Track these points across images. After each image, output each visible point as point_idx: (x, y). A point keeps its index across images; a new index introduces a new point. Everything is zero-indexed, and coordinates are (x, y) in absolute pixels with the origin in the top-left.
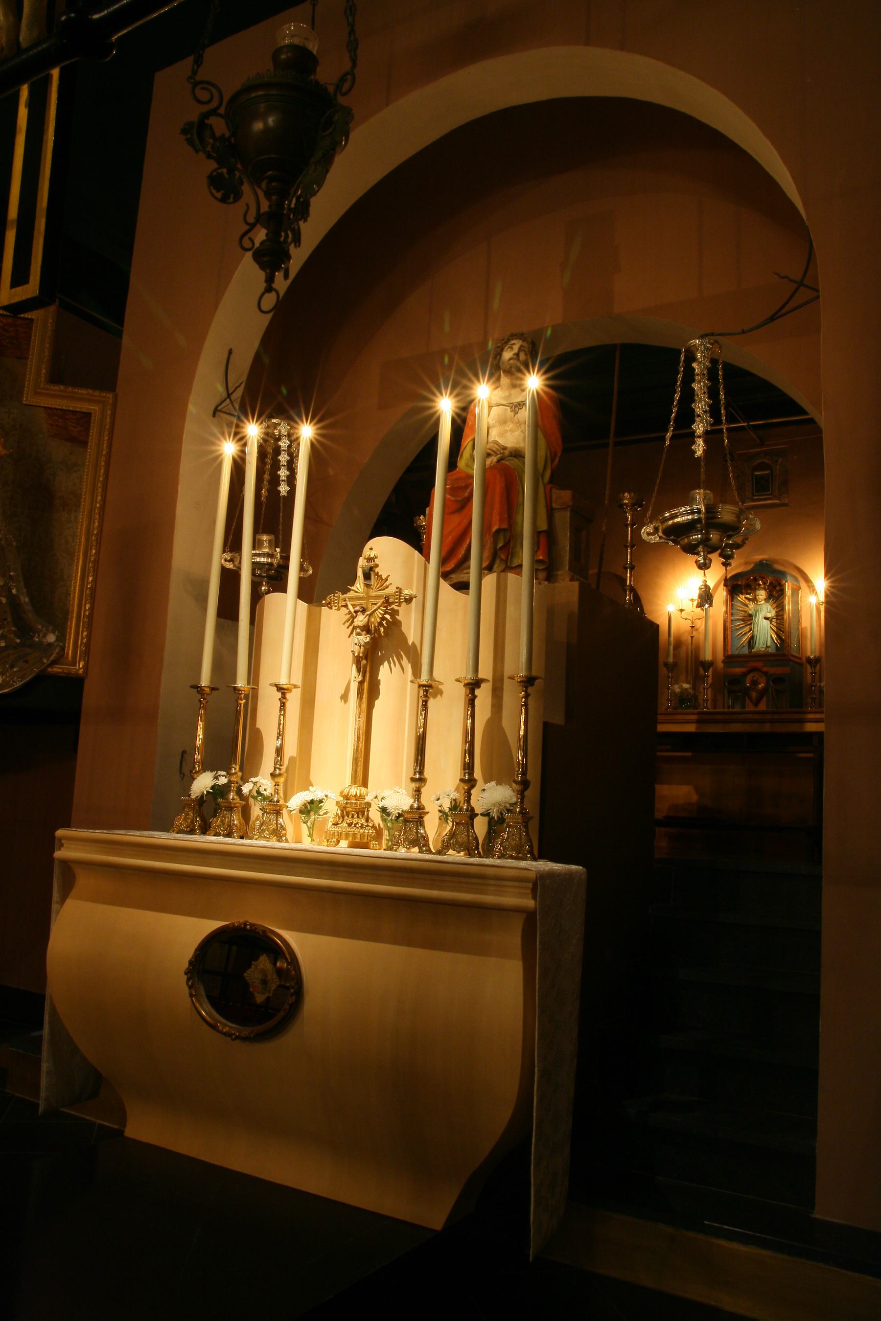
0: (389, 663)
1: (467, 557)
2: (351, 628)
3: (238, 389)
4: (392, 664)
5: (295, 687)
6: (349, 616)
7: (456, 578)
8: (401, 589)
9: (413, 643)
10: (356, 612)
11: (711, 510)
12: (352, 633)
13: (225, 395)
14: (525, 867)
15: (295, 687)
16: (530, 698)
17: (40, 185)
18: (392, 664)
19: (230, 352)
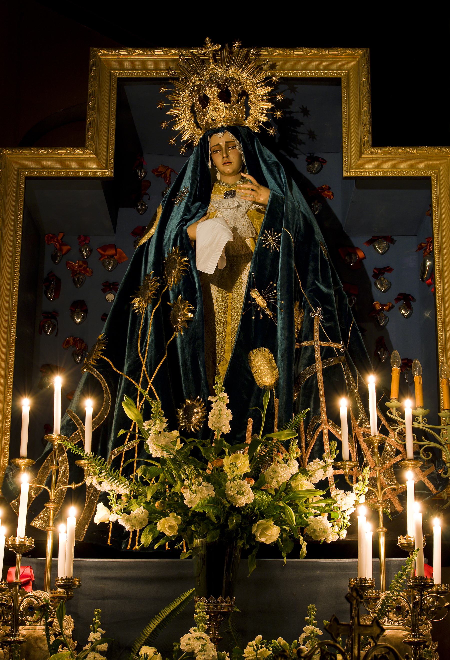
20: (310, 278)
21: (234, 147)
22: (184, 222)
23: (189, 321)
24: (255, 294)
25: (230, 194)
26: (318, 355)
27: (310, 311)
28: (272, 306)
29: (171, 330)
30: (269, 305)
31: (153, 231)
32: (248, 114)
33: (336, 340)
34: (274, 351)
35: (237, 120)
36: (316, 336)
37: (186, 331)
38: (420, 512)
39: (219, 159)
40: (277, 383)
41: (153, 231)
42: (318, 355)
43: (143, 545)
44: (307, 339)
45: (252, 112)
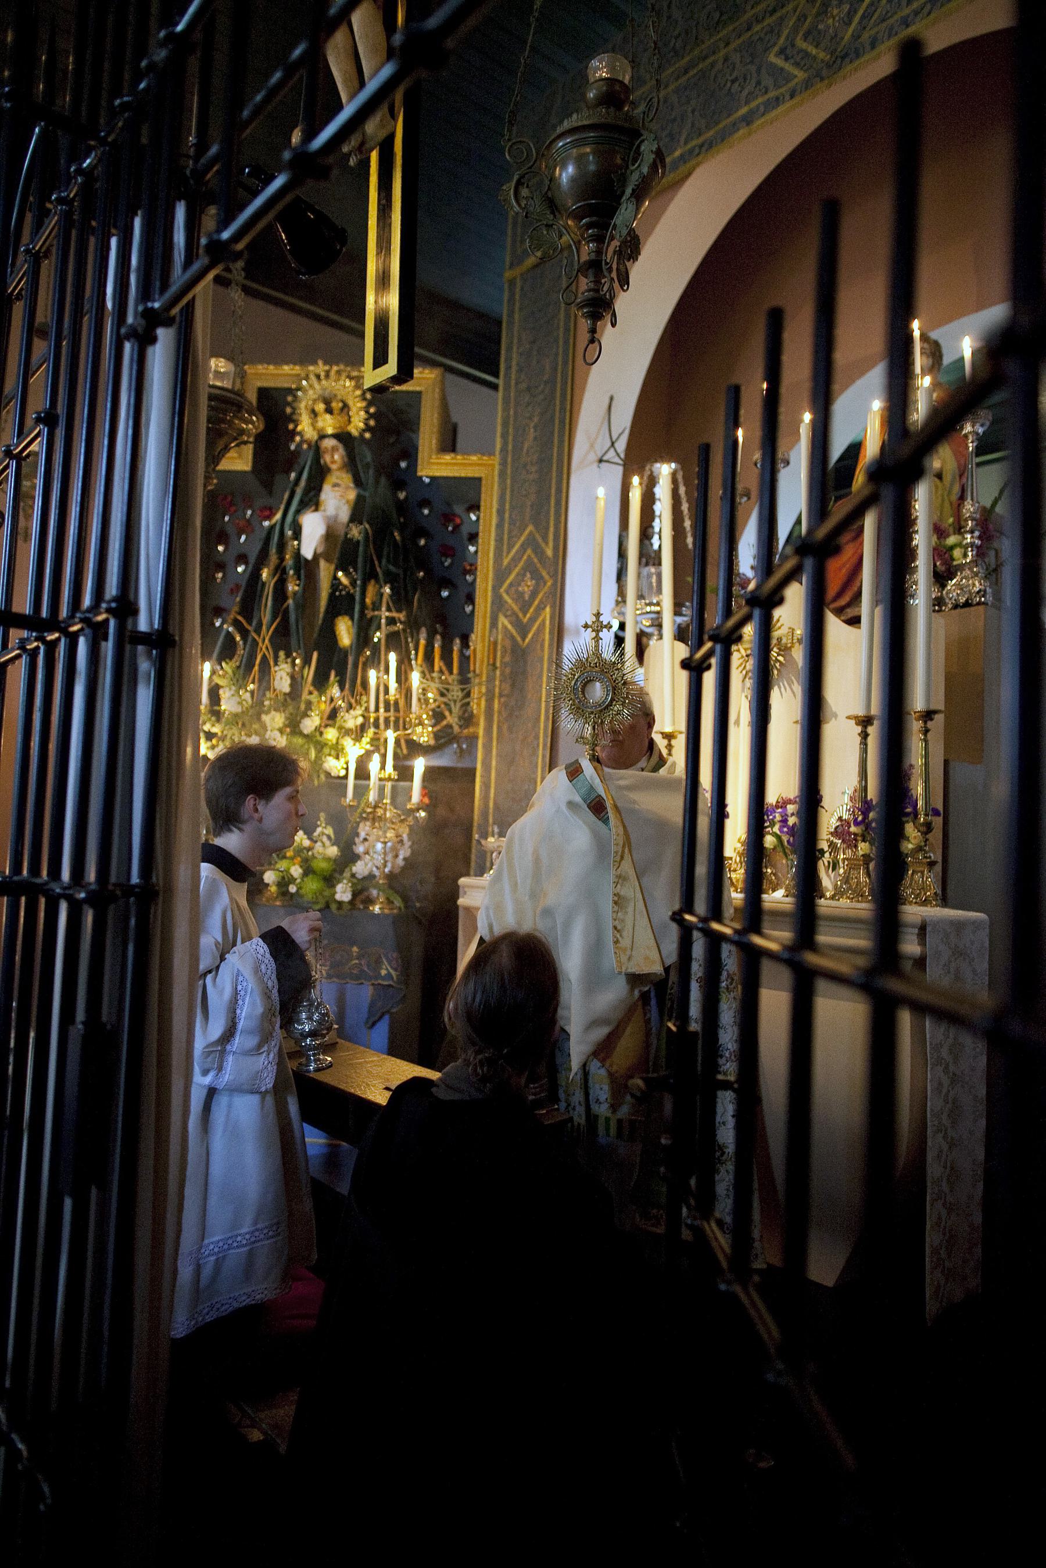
0: (780, 688)
1: (859, 594)
2: (744, 672)
3: (622, 437)
4: (783, 689)
5: (681, 733)
6: (741, 661)
7: (850, 613)
8: (793, 630)
9: (871, 800)
10: (747, 656)
11: (576, 137)
12: (745, 677)
13: (609, 444)
14: (728, 514)
15: (681, 733)
16: (929, 735)
17: (67, 530)
18: (783, 689)
19: (612, 398)
20: (384, 561)
21: (337, 450)
22: (298, 512)
23: (295, 593)
24: (340, 574)
25: (335, 485)
26: (383, 621)
27: (381, 587)
28: (353, 583)
29: (285, 598)
30: (351, 583)
31: (278, 516)
32: (350, 422)
33: (399, 611)
34: (352, 618)
35: (340, 427)
36: (384, 609)
37: (294, 599)
38: (860, 628)
39: (327, 458)
40: (351, 646)
41: (278, 516)
42: (383, 621)
43: (207, 877)
44: (377, 610)
45: (352, 419)
